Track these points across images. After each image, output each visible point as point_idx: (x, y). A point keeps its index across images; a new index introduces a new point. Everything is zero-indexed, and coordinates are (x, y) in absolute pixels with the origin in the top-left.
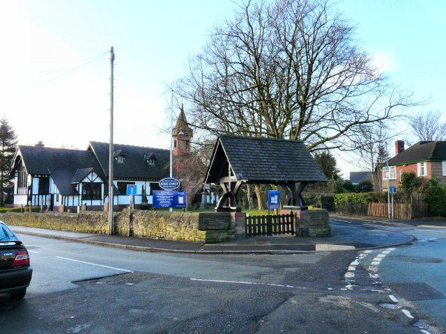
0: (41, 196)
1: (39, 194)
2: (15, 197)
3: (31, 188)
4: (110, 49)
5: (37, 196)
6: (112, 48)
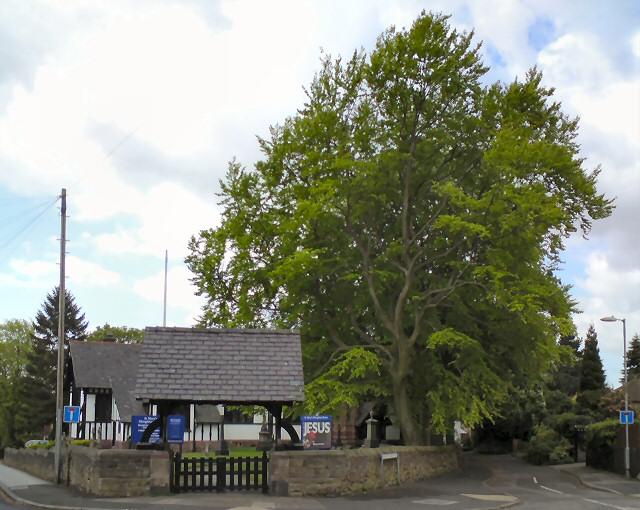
0: (98, 425)
1: (95, 422)
4: (60, 194)
5: (93, 426)
6: (64, 191)
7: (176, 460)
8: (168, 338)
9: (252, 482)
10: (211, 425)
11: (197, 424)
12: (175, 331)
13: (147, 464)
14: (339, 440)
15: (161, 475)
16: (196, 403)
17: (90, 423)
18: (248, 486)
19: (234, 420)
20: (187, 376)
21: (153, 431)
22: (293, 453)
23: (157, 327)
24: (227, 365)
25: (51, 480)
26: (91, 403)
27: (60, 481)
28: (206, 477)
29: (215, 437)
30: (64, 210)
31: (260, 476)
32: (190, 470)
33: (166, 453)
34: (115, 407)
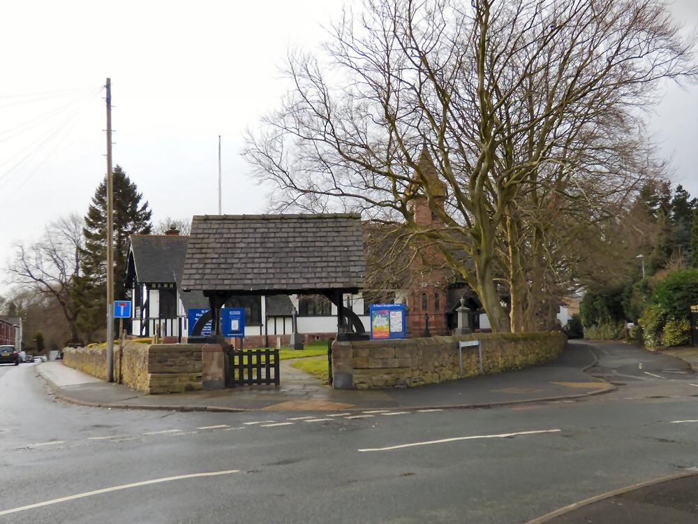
0: (163, 321)
1: (160, 319)
2: (133, 322)
3: (147, 306)
4: (105, 84)
6: (109, 80)
7: (229, 352)
8: (217, 226)
9: (255, 377)
10: (284, 317)
11: (268, 317)
12: (225, 219)
13: (199, 359)
14: (427, 330)
15: (216, 371)
16: (269, 293)
17: (136, 319)
18: (259, 381)
19: (310, 313)
20: (239, 266)
21: (204, 325)
22: (356, 343)
23: (207, 216)
24: (281, 252)
25: (104, 378)
26: (154, 299)
27: (112, 380)
28: (263, 370)
29: (289, 331)
30: (108, 100)
31: (272, 370)
32: (272, 363)
33: (218, 346)
34: (180, 303)
